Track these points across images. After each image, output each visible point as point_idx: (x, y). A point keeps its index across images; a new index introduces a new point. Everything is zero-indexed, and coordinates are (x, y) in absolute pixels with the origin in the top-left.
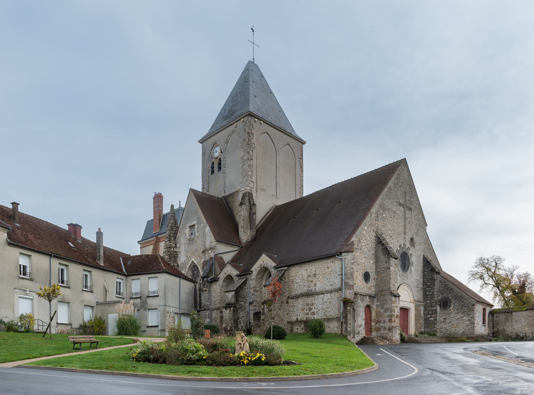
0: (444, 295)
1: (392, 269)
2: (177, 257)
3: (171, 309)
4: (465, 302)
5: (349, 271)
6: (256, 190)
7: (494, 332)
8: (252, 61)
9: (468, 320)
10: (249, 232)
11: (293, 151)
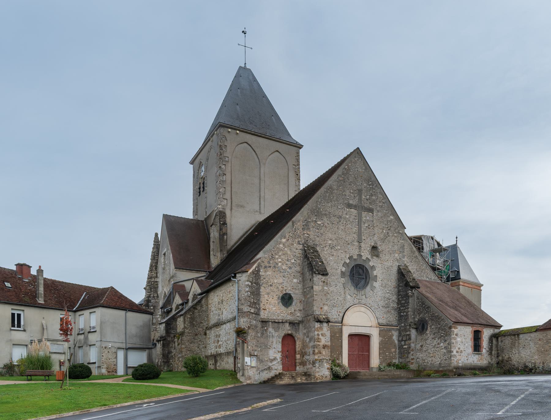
0: (421, 316)
1: (316, 288)
2: (157, 287)
3: (110, 345)
4: (442, 324)
5: (243, 296)
6: (230, 208)
7: (499, 362)
8: (243, 66)
9: (445, 348)
10: (219, 254)
11: (285, 158)
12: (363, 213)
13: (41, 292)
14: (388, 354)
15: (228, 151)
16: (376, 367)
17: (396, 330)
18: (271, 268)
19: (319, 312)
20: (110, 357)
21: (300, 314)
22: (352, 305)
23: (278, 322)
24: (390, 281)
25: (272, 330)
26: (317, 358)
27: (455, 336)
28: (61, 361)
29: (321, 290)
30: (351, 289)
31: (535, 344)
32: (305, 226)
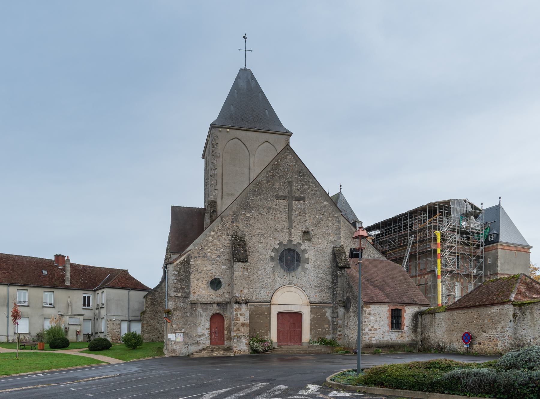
6: (221, 197)
7: (422, 340)
8: (243, 68)
12: (293, 202)
13: (68, 277)
14: (320, 329)
15: (219, 148)
16: (307, 342)
17: (330, 308)
18: (201, 258)
19: (239, 294)
20: (114, 328)
21: (228, 296)
22: (282, 285)
23: (207, 304)
24: (323, 262)
25: (201, 310)
26: (235, 335)
27: (367, 315)
28: (78, 331)
29: (241, 275)
30: (280, 272)
31: (445, 323)
32: (234, 219)
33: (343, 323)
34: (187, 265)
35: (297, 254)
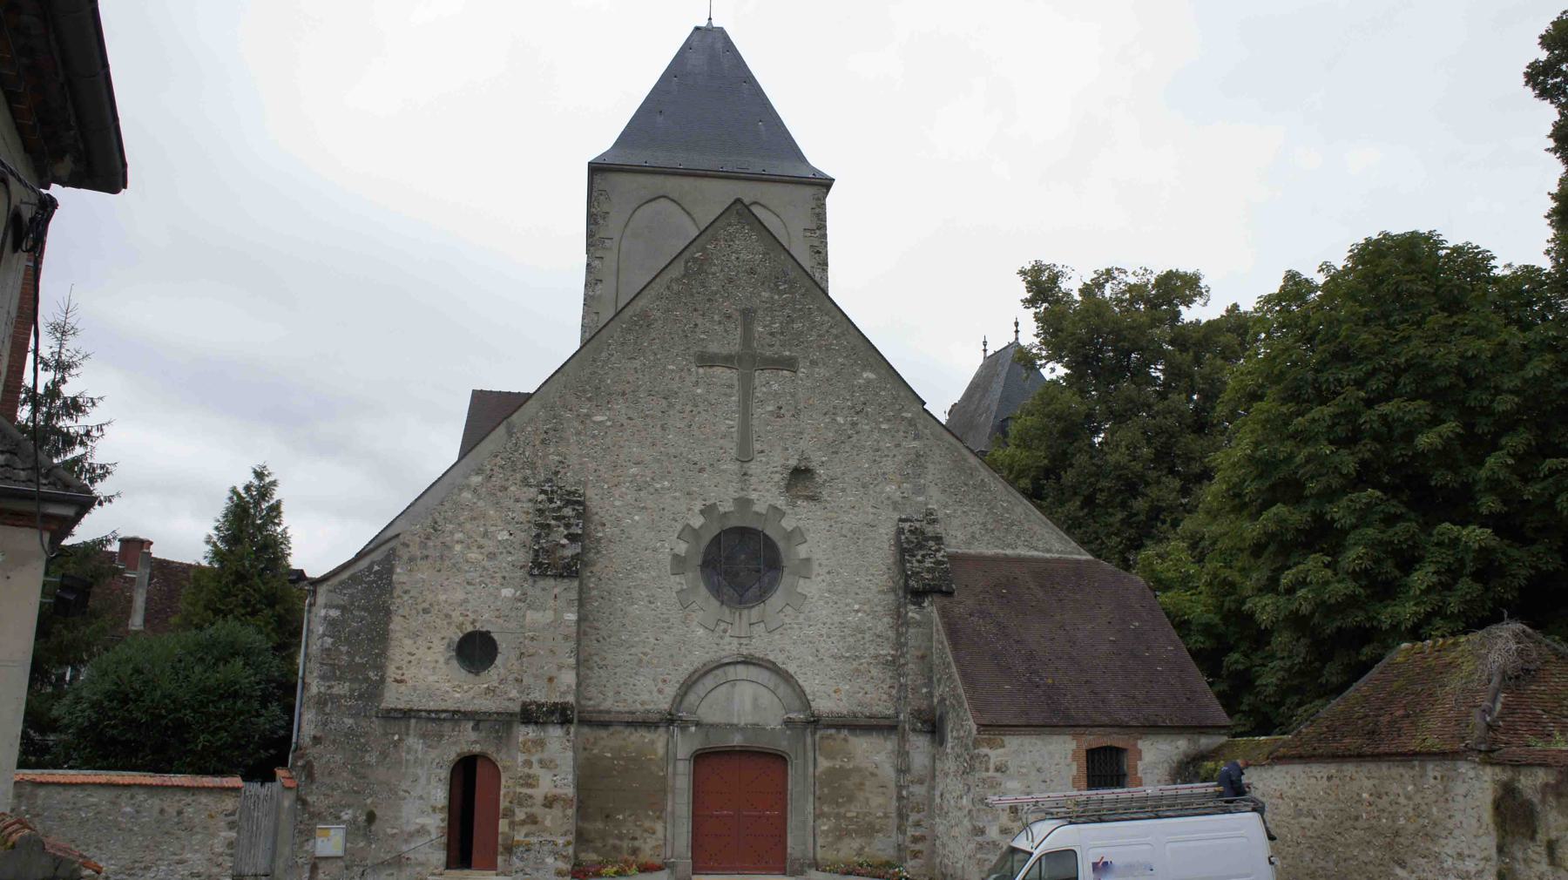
18: (430, 560)
33: (929, 792)
34: (378, 586)
35: (770, 544)
